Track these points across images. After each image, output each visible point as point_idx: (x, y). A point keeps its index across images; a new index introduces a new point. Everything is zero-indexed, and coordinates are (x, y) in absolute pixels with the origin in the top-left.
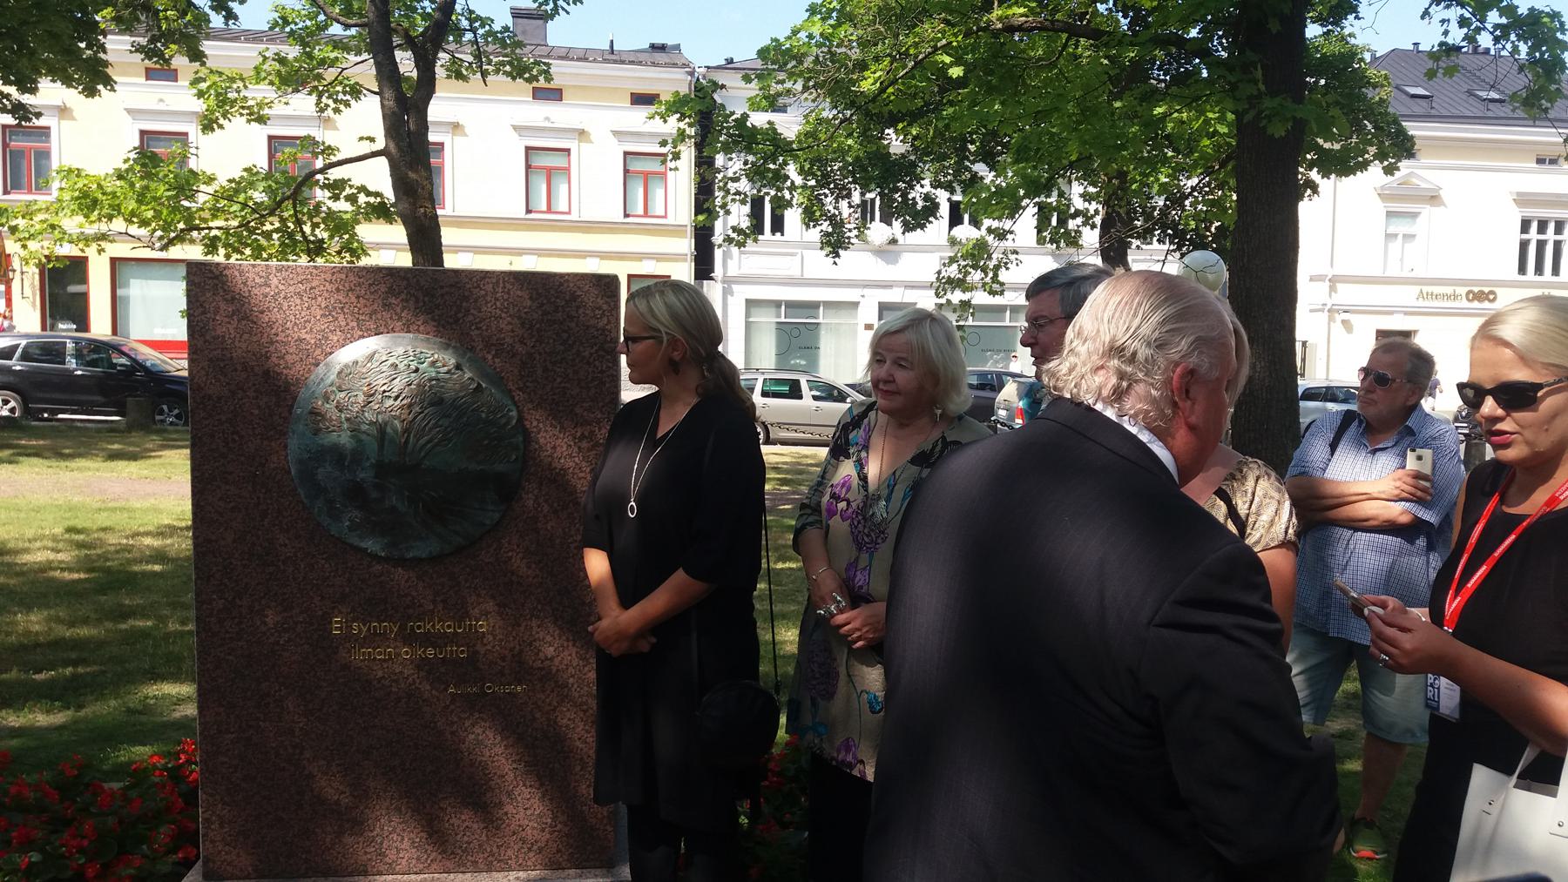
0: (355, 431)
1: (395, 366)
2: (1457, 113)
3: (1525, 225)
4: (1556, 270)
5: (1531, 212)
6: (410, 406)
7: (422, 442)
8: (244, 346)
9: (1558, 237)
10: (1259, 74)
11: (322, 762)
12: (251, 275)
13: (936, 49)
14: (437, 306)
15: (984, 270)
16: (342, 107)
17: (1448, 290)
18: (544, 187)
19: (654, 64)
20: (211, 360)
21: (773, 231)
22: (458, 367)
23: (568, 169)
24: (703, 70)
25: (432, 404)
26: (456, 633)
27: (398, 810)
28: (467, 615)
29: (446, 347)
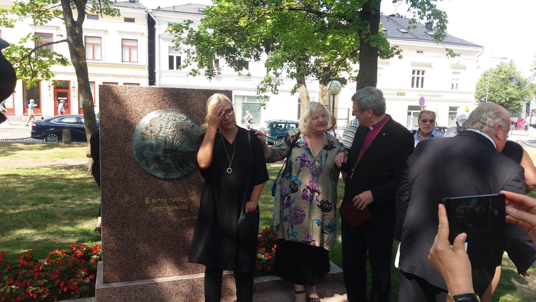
0: (156, 139)
1: (168, 119)
2: (394, 36)
3: (414, 72)
4: (422, 86)
5: (417, 68)
6: (174, 131)
7: (178, 142)
8: (118, 112)
9: (423, 76)
10: (369, 27)
11: (142, 244)
12: (120, 89)
13: (265, 14)
14: (179, 100)
15: (272, 86)
16: (44, 23)
17: (392, 92)
18: (92, 50)
19: (133, 8)
20: (107, 117)
21: (177, 68)
22: (187, 119)
23: (137, 47)
24: (151, 11)
25: (180, 131)
26: (184, 201)
27: (166, 257)
28: (187, 195)
29: (182, 112)
